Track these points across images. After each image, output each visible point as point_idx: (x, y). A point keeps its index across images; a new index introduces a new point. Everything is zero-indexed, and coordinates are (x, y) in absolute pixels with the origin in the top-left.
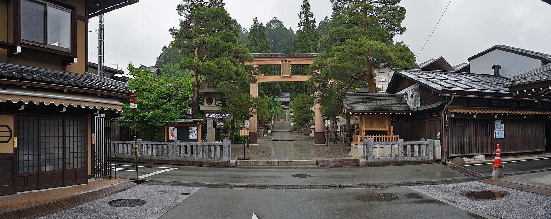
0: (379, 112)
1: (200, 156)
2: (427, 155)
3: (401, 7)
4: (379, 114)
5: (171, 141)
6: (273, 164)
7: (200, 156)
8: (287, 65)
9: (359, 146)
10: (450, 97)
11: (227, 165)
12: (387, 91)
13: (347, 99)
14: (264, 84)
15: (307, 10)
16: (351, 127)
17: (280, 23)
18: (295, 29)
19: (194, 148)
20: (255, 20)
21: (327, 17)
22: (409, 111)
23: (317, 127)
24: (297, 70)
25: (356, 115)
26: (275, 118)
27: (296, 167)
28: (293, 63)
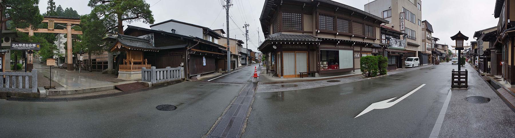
1: (7, 86)
6: (80, 92)
7: (7, 86)
10: (197, 42)
11: (37, 97)
28: (55, 22)
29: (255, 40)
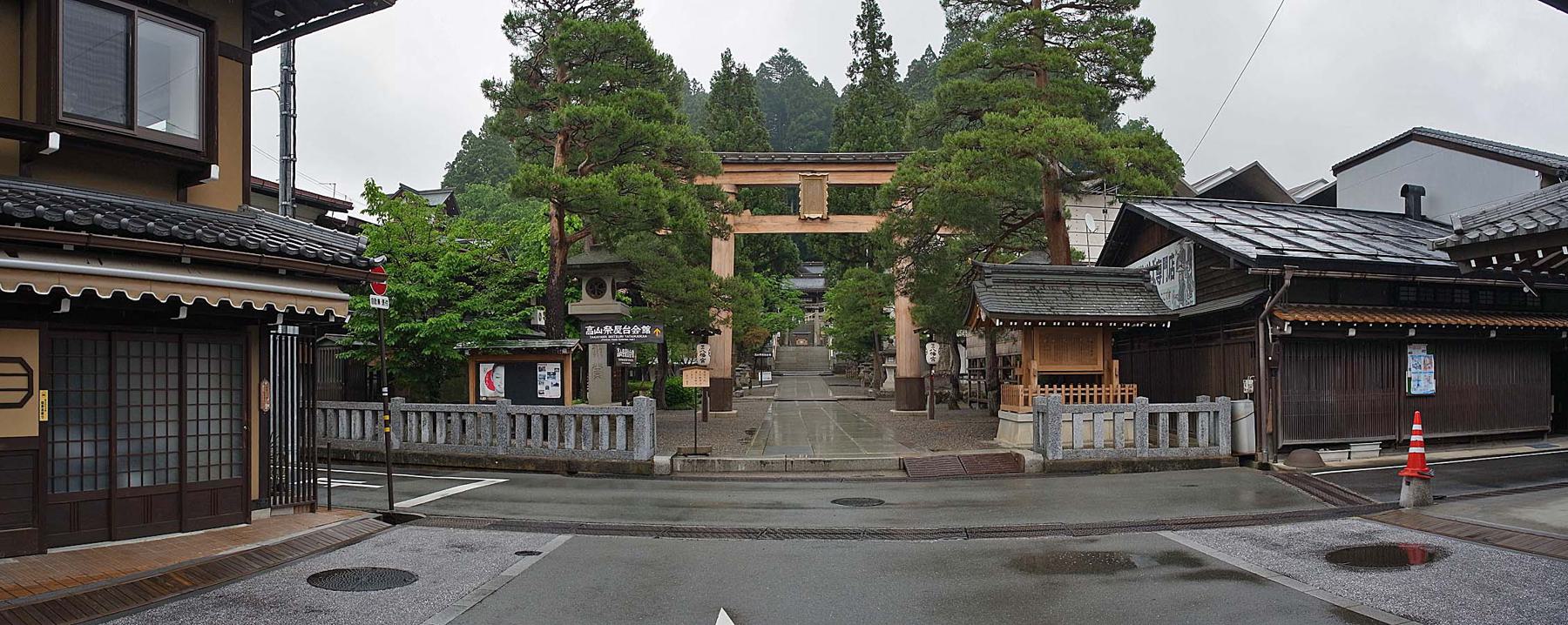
0: (1079, 320)
1: (570, 444)
2: (1214, 443)
3: (1142, 21)
4: (1078, 324)
5: (487, 402)
6: (776, 467)
7: (570, 444)
8: (817, 184)
9: (1020, 418)
10: (1281, 278)
11: (646, 471)
12: (1102, 261)
13: (989, 282)
14: (750, 239)
15: (873, 28)
16: (1000, 363)
17: (797, 64)
18: (840, 84)
19: (553, 422)
20: (727, 58)
21: (929, 48)
22: (1164, 318)
23: (903, 363)
24: (844, 201)
25: (1013, 327)
26: (783, 337)
27: (841, 475)
28: (835, 179)
29: (1094, 254)
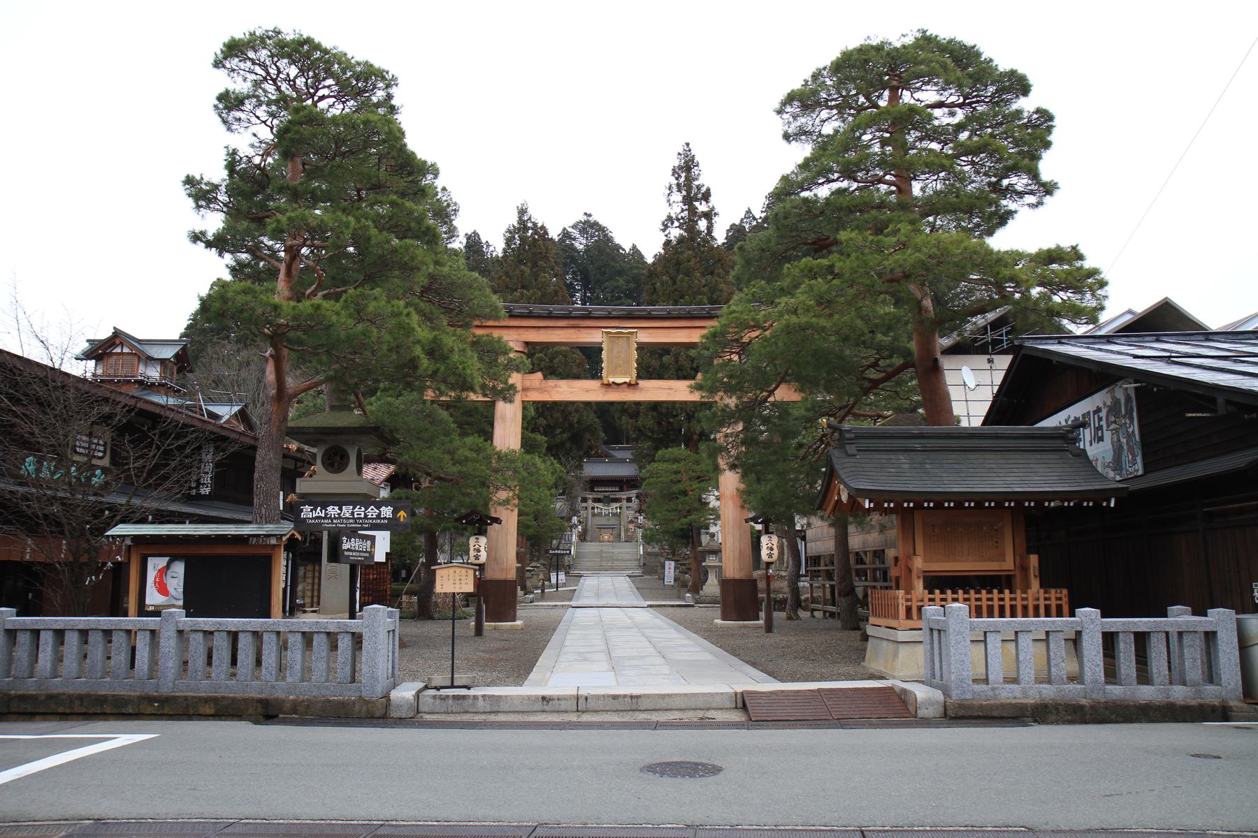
0: (979, 498)
2: (1211, 675)
3: (1038, 111)
4: (979, 505)
5: (156, 613)
8: (622, 342)
9: (902, 636)
12: (989, 419)
13: (851, 449)
14: (544, 409)
15: (689, 180)
16: (852, 560)
17: (602, 229)
18: (651, 249)
19: (245, 642)
20: (522, 212)
21: (749, 212)
22: (1106, 494)
23: (731, 563)
24: (656, 362)
25: (887, 511)
26: (585, 531)
27: (655, 717)
28: (645, 337)
